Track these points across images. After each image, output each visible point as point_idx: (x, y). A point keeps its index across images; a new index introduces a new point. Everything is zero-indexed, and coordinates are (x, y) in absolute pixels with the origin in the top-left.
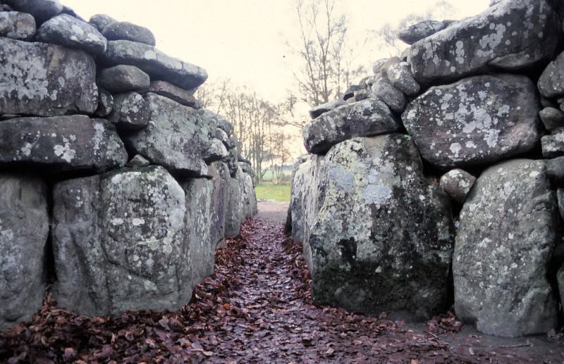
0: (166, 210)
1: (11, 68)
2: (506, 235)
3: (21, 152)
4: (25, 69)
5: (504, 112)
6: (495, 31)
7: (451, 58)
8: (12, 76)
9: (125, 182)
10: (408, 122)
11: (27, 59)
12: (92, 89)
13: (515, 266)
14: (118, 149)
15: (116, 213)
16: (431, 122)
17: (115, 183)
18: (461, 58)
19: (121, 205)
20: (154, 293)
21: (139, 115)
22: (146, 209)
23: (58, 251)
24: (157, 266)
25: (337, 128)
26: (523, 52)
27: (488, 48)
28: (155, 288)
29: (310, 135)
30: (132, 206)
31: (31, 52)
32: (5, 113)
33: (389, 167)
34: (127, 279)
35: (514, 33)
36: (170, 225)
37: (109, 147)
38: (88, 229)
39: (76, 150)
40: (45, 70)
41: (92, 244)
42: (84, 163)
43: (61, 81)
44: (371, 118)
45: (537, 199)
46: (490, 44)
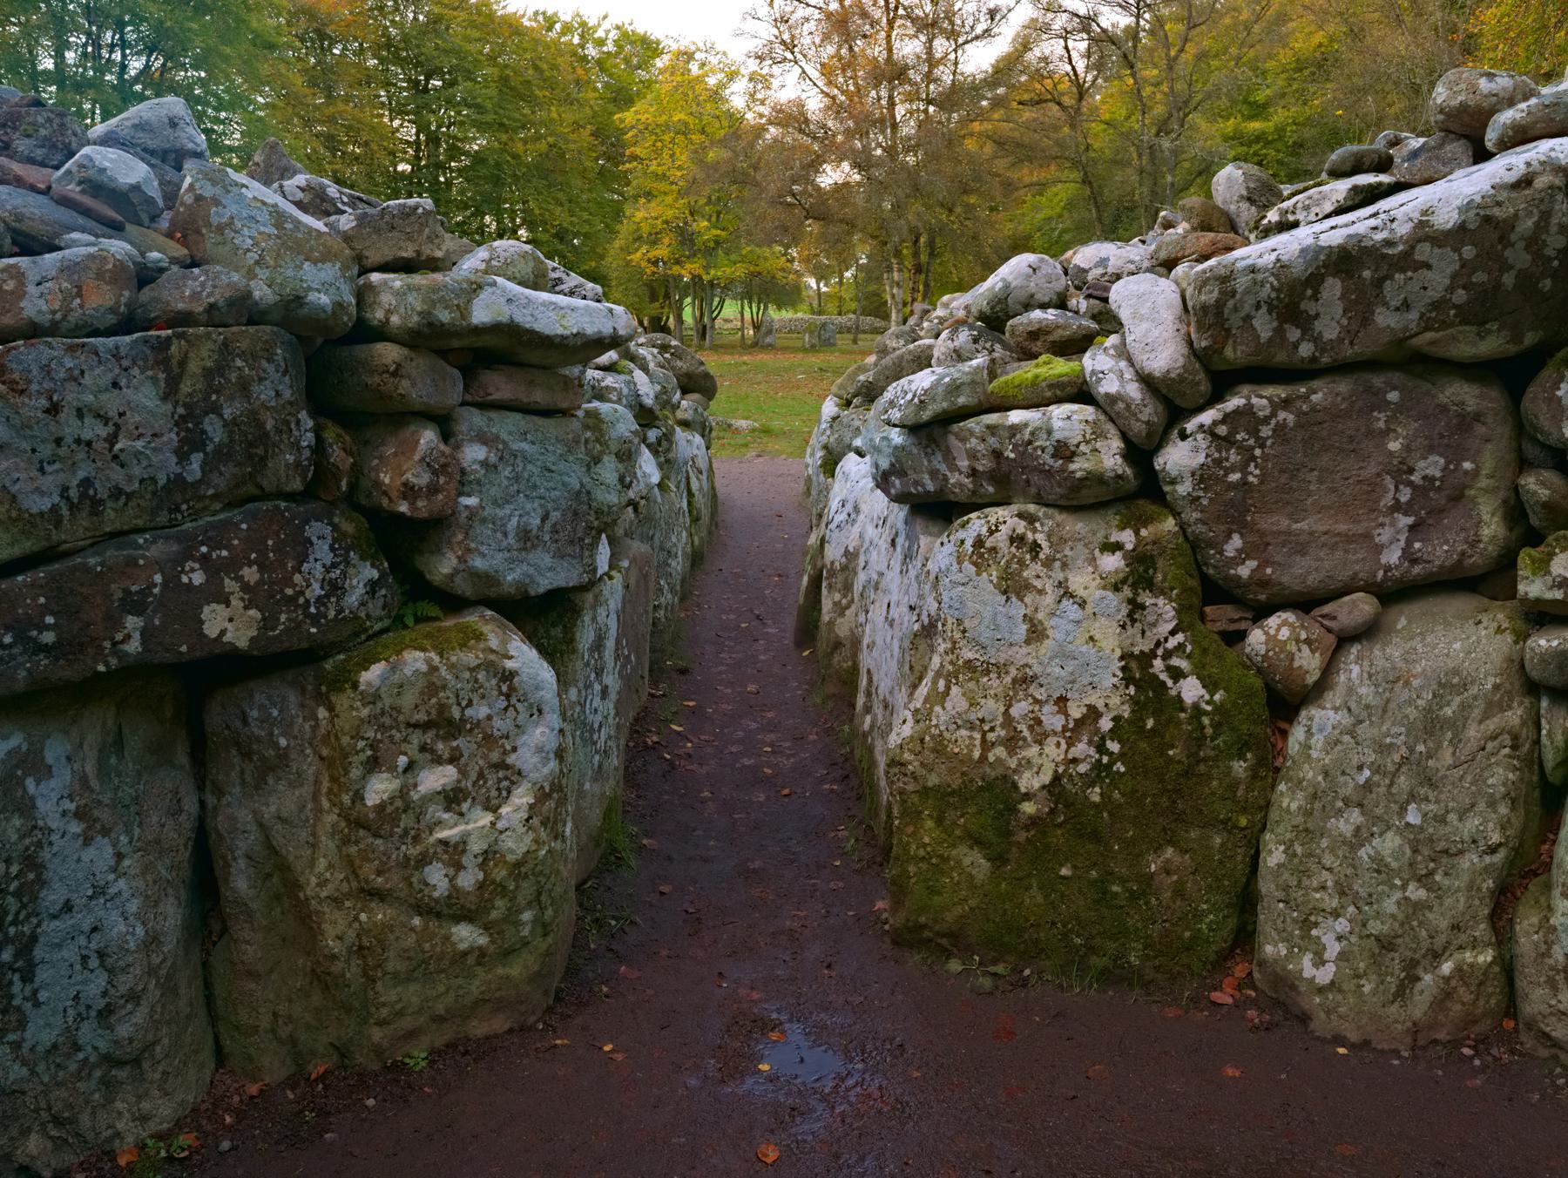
2: (1403, 810)
4: (113, 413)
7: (1305, 322)
8: (78, 441)
11: (115, 385)
13: (1416, 893)
20: (482, 952)
21: (433, 489)
22: (454, 744)
25: (973, 473)
27: (1406, 306)
28: (483, 940)
29: (892, 465)
30: (416, 738)
35: (1480, 277)
43: (214, 429)
44: (1073, 467)
45: (1492, 725)
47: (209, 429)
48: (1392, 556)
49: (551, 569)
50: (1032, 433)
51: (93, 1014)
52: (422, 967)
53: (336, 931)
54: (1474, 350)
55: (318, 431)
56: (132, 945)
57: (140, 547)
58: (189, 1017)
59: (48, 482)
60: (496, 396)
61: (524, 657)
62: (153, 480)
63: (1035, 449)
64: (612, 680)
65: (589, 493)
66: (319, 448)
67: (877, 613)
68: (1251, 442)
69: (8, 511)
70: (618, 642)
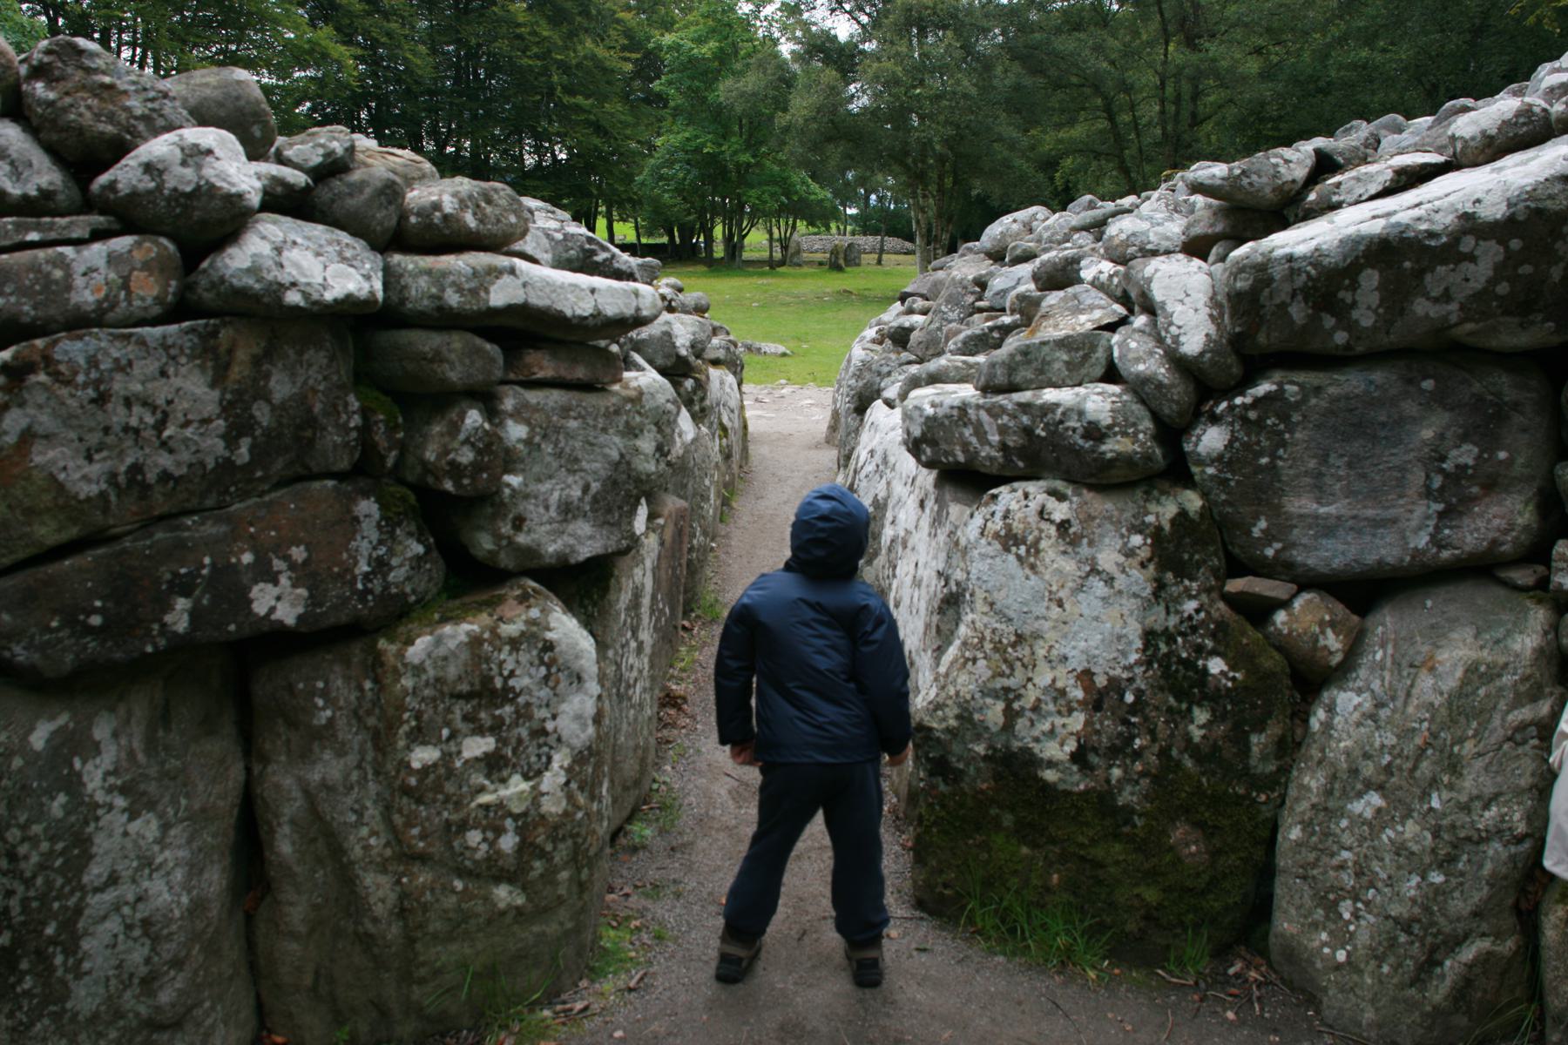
0: (547, 705)
1: (122, 410)
2: (1425, 796)
3: (164, 625)
4: (161, 401)
5: (1462, 460)
6: (1472, 258)
7: (1342, 312)
8: (127, 429)
9: (442, 651)
10: (1201, 462)
12: (346, 412)
13: (1437, 878)
14: (418, 558)
15: (420, 735)
16: (1261, 469)
17: (416, 661)
18: (1370, 313)
19: (431, 711)
21: (477, 467)
22: (497, 712)
23: (272, 831)
24: (526, 847)
26: (1539, 317)
27: (1446, 297)
29: (923, 434)
30: (459, 710)
31: (173, 352)
32: (114, 526)
33: (1139, 580)
34: (453, 891)
35: (1526, 269)
36: (559, 740)
37: (394, 562)
38: (347, 776)
39: (309, 589)
40: (216, 394)
41: (360, 813)
42: (332, 620)
43: (262, 414)
44: (1104, 448)
46: (1453, 290)
47: (257, 414)
48: (1422, 540)
49: (590, 538)
50: (1064, 414)
51: (136, 981)
52: (459, 924)
53: (378, 888)
54: (1515, 340)
55: (365, 412)
56: (177, 913)
57: (188, 528)
58: (231, 978)
59: (95, 469)
60: (540, 375)
61: (565, 628)
62: (202, 464)
63: (1067, 429)
64: (646, 636)
65: (628, 463)
66: (366, 429)
67: (904, 569)
68: (1282, 427)
69: (55, 498)
70: (654, 597)
